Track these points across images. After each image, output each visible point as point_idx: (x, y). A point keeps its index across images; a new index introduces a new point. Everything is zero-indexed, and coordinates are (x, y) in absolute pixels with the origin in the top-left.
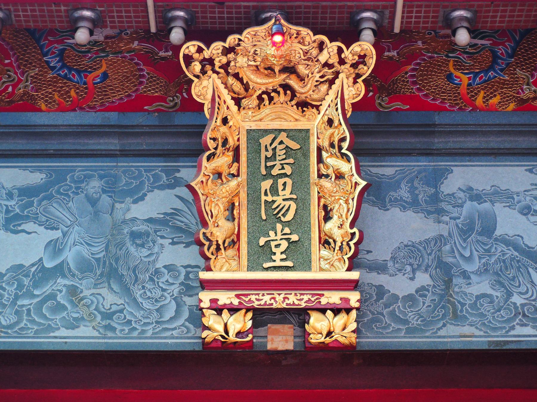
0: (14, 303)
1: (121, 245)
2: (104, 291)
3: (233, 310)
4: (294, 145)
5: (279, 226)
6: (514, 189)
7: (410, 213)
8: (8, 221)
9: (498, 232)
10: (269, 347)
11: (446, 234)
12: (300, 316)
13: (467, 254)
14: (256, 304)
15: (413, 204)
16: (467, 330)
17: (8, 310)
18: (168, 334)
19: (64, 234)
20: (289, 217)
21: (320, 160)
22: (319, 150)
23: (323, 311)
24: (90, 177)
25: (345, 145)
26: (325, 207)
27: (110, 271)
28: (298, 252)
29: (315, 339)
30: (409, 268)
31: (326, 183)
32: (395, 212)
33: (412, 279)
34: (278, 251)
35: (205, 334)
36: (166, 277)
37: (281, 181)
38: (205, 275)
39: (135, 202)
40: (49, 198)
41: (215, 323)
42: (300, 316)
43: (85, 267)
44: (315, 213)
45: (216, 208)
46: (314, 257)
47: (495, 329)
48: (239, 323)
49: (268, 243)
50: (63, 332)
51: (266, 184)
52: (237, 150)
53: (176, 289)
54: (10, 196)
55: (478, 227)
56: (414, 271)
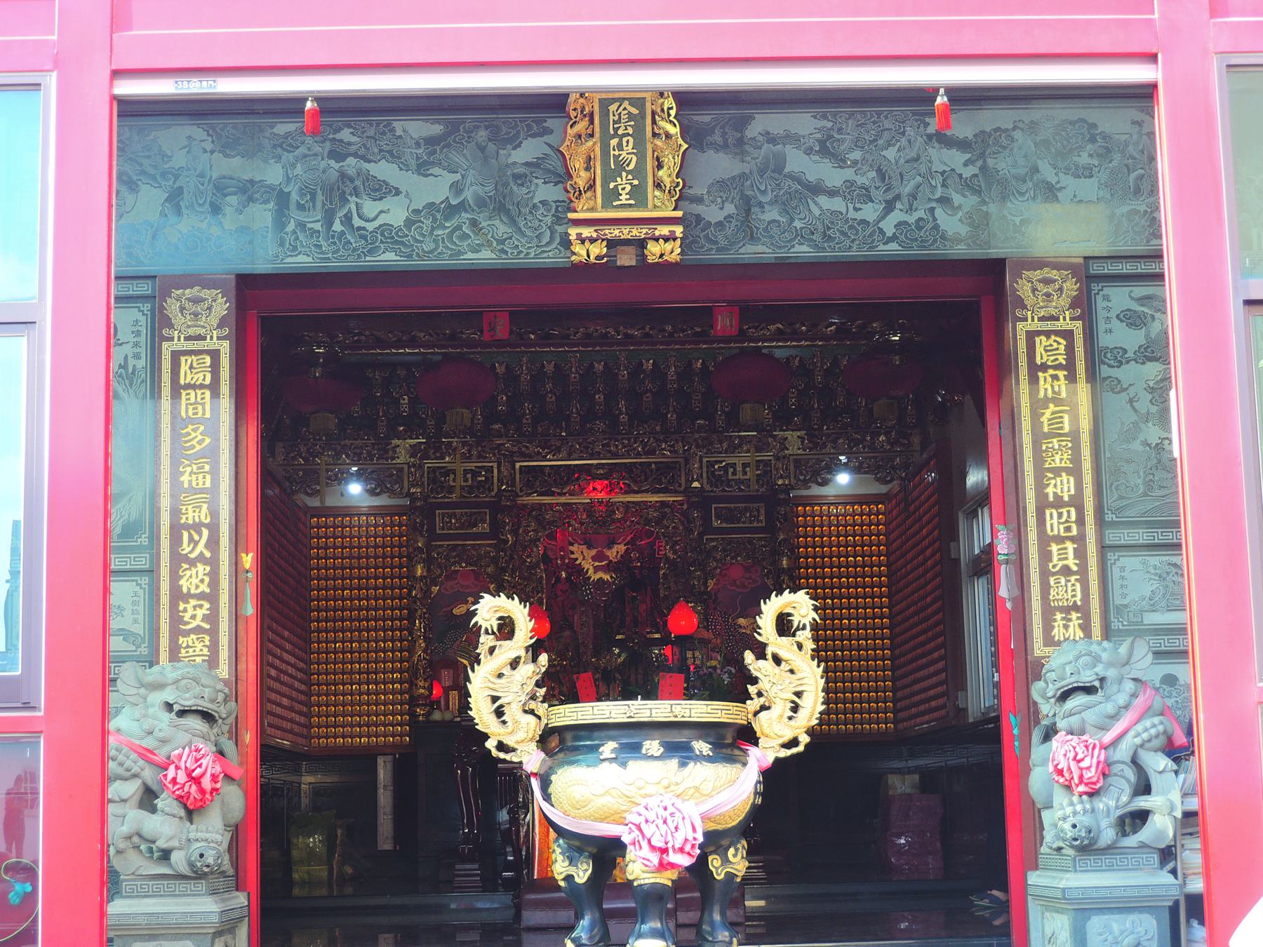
0: (431, 233)
1: (506, 185)
2: (497, 222)
3: (593, 240)
4: (635, 111)
5: (624, 174)
6: (801, 133)
7: (721, 154)
8: (419, 166)
9: (786, 170)
10: (618, 263)
11: (747, 172)
12: (641, 244)
13: (763, 188)
14: (609, 237)
15: (725, 147)
16: (760, 248)
17: (428, 239)
18: (545, 255)
19: (463, 177)
20: (632, 166)
21: (654, 122)
22: (653, 113)
23: (657, 240)
24: (477, 127)
25: (673, 112)
26: (658, 159)
27: (500, 205)
28: (638, 194)
29: (650, 259)
30: (719, 200)
31: (658, 142)
32: (711, 153)
33: (722, 209)
34: (623, 193)
35: (573, 258)
36: (542, 210)
37: (625, 140)
38: (571, 216)
39: (514, 148)
40: (448, 146)
41: (580, 252)
42: (641, 244)
43: (481, 203)
44: (650, 164)
45: (577, 164)
46: (650, 196)
47: (780, 247)
48: (597, 250)
49: (616, 186)
50: (470, 255)
51: (614, 142)
52: (591, 115)
53: (549, 220)
54: (418, 145)
55: (772, 166)
56: (723, 202)
